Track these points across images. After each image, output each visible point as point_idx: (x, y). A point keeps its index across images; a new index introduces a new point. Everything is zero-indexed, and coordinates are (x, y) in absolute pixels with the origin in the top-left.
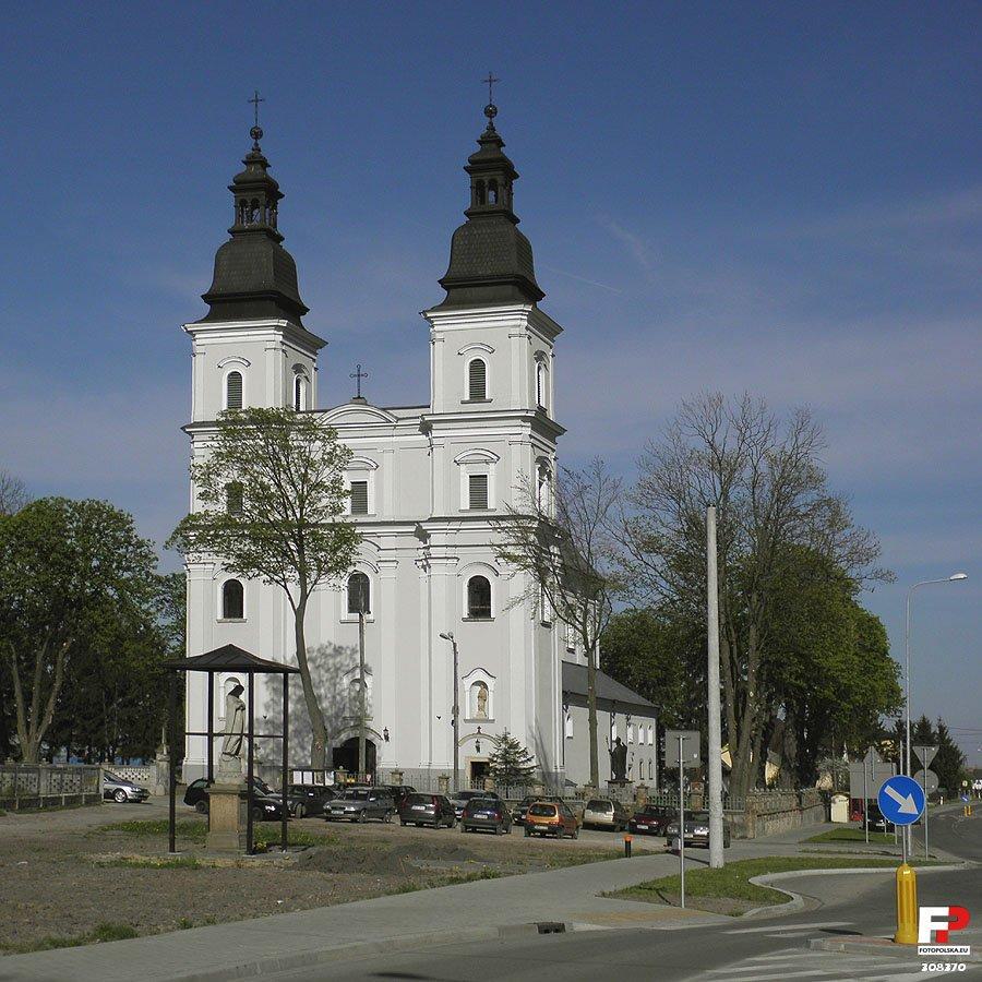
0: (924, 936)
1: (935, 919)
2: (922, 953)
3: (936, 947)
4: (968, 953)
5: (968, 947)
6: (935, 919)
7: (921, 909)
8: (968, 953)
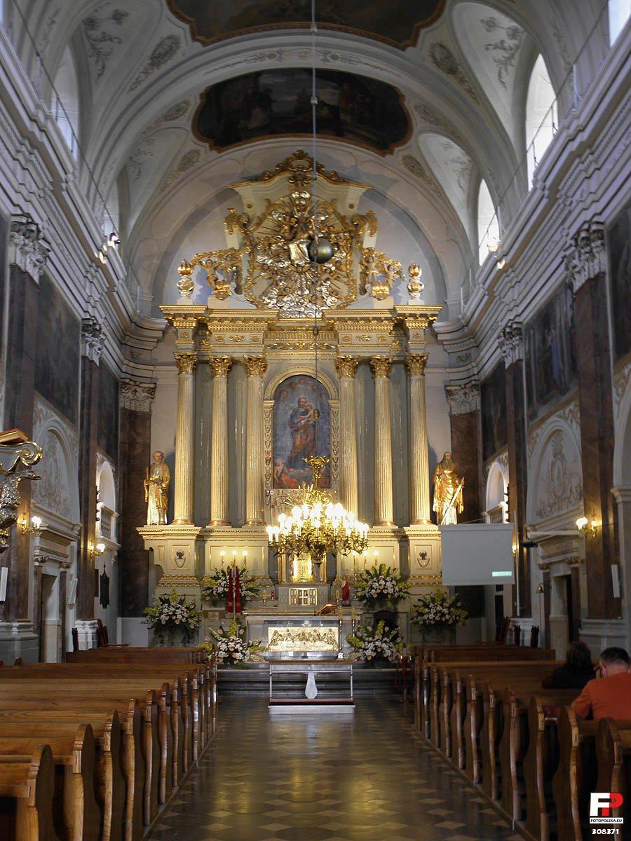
0: (594, 811)
1: (601, 800)
2: (592, 823)
3: (601, 819)
4: (622, 822)
5: (622, 819)
6: (601, 800)
7: (592, 794)
8: (622, 822)
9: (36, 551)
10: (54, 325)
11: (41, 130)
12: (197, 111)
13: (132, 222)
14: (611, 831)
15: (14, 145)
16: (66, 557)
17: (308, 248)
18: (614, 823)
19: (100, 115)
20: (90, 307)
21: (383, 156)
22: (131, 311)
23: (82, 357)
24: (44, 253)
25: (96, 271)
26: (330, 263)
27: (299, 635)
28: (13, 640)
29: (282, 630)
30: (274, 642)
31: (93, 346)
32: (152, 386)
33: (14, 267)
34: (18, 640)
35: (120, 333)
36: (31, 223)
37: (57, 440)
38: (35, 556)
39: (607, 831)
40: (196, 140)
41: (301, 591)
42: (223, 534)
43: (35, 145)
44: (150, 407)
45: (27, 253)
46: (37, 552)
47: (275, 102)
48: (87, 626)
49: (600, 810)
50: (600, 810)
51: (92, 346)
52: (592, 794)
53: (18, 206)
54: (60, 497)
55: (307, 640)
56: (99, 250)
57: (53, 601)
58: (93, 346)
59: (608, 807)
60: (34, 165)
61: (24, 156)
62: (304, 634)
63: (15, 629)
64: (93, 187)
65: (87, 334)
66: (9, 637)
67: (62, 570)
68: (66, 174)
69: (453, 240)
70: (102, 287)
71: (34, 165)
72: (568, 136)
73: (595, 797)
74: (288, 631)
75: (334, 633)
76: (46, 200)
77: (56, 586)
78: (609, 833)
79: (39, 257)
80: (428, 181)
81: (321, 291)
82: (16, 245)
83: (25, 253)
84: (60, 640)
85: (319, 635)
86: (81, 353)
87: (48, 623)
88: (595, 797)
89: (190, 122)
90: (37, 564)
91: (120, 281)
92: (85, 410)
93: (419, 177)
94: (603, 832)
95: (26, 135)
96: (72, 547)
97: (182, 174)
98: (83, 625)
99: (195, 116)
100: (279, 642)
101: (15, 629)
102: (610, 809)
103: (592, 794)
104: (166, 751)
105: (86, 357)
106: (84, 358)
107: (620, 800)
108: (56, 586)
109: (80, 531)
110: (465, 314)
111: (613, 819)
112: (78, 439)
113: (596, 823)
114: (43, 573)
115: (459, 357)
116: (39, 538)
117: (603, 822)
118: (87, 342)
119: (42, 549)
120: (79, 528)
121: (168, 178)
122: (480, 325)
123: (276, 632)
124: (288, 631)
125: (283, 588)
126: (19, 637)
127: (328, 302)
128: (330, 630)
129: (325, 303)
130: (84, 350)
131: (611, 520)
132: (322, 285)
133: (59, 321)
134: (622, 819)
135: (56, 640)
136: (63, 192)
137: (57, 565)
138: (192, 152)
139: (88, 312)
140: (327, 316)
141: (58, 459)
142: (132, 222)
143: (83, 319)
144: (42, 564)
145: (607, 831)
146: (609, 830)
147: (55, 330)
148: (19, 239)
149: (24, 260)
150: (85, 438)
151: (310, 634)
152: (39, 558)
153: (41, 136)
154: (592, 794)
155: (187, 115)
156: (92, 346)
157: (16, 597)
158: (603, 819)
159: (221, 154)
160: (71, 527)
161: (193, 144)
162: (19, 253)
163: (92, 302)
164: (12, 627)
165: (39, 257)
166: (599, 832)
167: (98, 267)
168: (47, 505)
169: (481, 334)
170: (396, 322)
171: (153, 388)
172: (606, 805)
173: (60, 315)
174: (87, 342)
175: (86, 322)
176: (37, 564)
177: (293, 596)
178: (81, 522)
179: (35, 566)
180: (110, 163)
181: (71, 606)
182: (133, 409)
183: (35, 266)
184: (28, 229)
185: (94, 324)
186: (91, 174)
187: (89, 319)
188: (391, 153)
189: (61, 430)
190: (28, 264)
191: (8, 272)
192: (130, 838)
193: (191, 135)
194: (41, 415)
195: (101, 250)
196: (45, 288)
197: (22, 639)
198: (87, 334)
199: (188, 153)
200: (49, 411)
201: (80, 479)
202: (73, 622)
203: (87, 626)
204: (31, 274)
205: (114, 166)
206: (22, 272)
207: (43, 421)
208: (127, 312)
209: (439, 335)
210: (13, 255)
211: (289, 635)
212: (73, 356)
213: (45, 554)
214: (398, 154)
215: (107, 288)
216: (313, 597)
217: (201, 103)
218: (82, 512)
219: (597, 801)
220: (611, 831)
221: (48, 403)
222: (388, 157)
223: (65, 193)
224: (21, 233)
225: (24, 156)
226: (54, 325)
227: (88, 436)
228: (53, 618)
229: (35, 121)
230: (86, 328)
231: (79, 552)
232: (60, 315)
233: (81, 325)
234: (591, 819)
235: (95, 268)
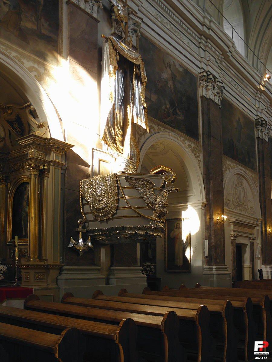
0: (256, 349)
1: (259, 345)
2: (255, 354)
3: (259, 352)
4: (268, 354)
5: (268, 352)
6: (259, 345)
7: (255, 342)
8: (268, 354)
9: (231, 232)
10: (235, 124)
11: (209, 29)
14: (264, 358)
15: (196, 40)
16: (253, 234)
18: (265, 354)
23: (257, 138)
24: (220, 88)
25: (261, 95)
28: (213, 274)
31: (263, 132)
33: (203, 97)
34: (215, 275)
36: (210, 75)
37: (243, 179)
38: (231, 234)
39: (262, 358)
43: (208, 37)
45: (209, 90)
46: (232, 232)
48: (268, 268)
49: (259, 349)
50: (259, 349)
51: (262, 132)
52: (255, 342)
53: (202, 68)
54: (248, 206)
56: (260, 84)
57: (247, 256)
58: (263, 132)
59: (262, 347)
60: (209, 48)
61: (203, 44)
63: (214, 269)
64: (256, 58)
65: (258, 126)
66: (211, 273)
67: (251, 241)
70: (266, 103)
71: (209, 48)
73: (256, 343)
76: (222, 64)
77: (248, 249)
78: (263, 358)
79: (218, 91)
82: (203, 87)
83: (208, 90)
84: (251, 275)
86: (256, 136)
87: (245, 267)
88: (256, 343)
90: (232, 238)
92: (261, 163)
94: (260, 358)
95: (201, 34)
96: (258, 230)
98: (265, 267)
101: (214, 269)
102: (263, 348)
103: (255, 342)
104: (226, 325)
106: (258, 138)
107: (267, 344)
108: (248, 249)
109: (262, 222)
111: (264, 352)
112: (257, 177)
113: (257, 354)
114: (236, 242)
116: (232, 226)
117: (260, 354)
118: (259, 130)
119: (234, 231)
120: (261, 221)
126: (216, 273)
130: (258, 134)
131: (264, 229)
134: (268, 352)
135: (249, 275)
136: (230, 58)
137: (248, 239)
139: (258, 116)
141: (245, 188)
143: (256, 120)
144: (235, 238)
145: (262, 358)
146: (263, 357)
148: (204, 83)
149: (208, 93)
150: (262, 176)
152: (233, 235)
153: (209, 32)
154: (255, 342)
157: (215, 254)
158: (260, 352)
160: (257, 220)
162: (204, 90)
163: (260, 110)
164: (213, 268)
165: (218, 91)
166: (258, 358)
167: (261, 93)
168: (238, 210)
172: (261, 347)
173: (239, 119)
174: (259, 130)
175: (257, 121)
176: (232, 238)
178: (262, 217)
179: (232, 239)
180: (264, 40)
181: (259, 258)
183: (266, 135)
184: (208, 78)
187: (259, 119)
189: (246, 175)
190: (212, 95)
191: (200, 100)
194: (230, 167)
195: (261, 84)
196: (227, 107)
197: (217, 274)
198: (258, 126)
200: (235, 165)
201: (260, 197)
202: (259, 265)
203: (268, 268)
204: (213, 99)
205: (267, 42)
206: (208, 99)
207: (231, 169)
210: (202, 91)
212: (251, 138)
213: (236, 233)
215: (270, 103)
219: (257, 345)
220: (264, 358)
221: (234, 161)
223: (231, 58)
224: (204, 80)
225: (203, 44)
226: (235, 124)
227: (263, 175)
228: (247, 264)
229: (204, 25)
230: (258, 123)
231: (262, 232)
232: (239, 119)
233: (255, 123)
234: (255, 352)
235: (260, 94)
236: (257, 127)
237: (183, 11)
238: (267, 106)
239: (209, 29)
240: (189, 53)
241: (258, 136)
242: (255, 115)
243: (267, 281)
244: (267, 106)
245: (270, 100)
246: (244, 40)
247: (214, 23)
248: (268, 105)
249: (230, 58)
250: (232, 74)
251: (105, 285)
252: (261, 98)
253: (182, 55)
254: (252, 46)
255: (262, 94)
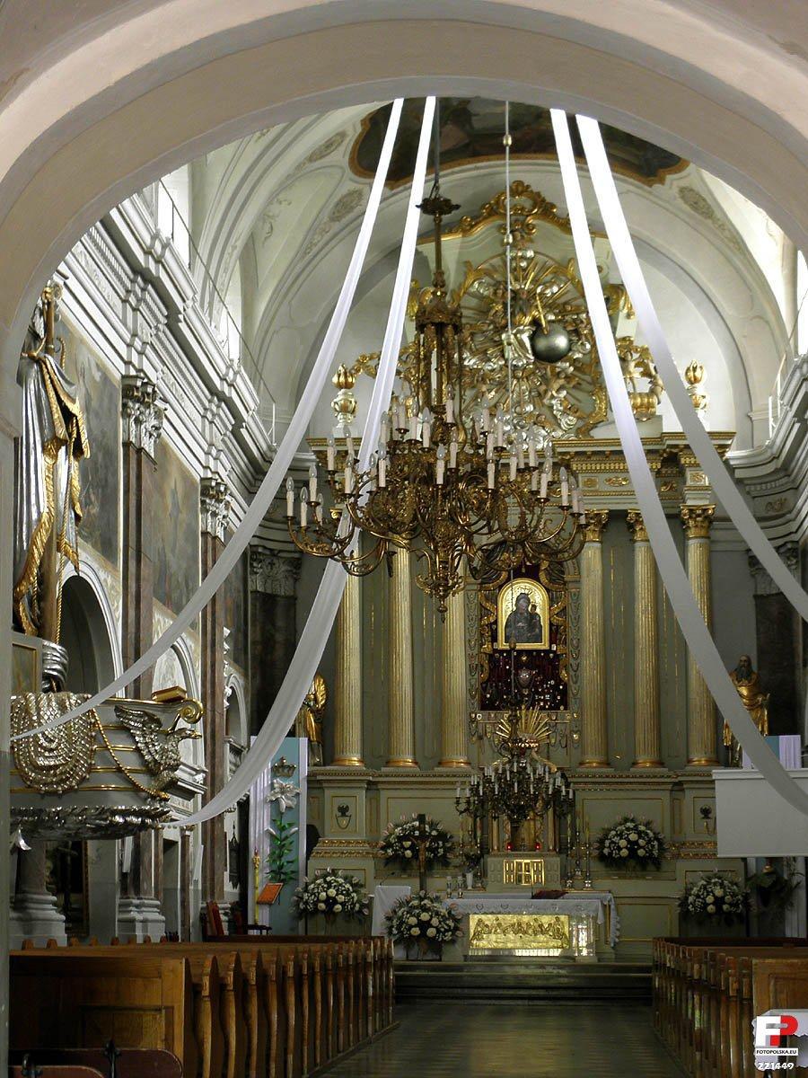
5: (797, 1049)
10: (169, 501)
12: (356, 142)
13: (261, 307)
17: (532, 338)
19: (218, 178)
20: (211, 459)
21: (651, 186)
22: (264, 447)
26: (566, 362)
27: (513, 925)
29: (489, 919)
30: (478, 935)
32: (297, 555)
35: (241, 468)
36: (147, 383)
40: (357, 178)
41: (521, 864)
42: (435, 779)
44: (294, 588)
47: (475, 115)
51: (138, 422)
55: (525, 933)
62: (520, 924)
64: (210, 284)
68: (184, 301)
69: (760, 317)
72: (772, 454)
74: (497, 919)
75: (562, 923)
80: (720, 226)
81: (551, 407)
85: (541, 926)
89: (347, 158)
91: (251, 412)
93: (706, 218)
95: (138, 270)
97: (336, 226)
99: (352, 152)
100: (485, 936)
105: (208, 533)
106: (205, 534)
110: (774, 442)
111: (785, 1049)
115: (770, 503)
118: (256, 573)
121: (314, 234)
122: (796, 459)
123: (480, 921)
124: (497, 919)
125: (493, 859)
127: (564, 426)
128: (558, 919)
129: (559, 425)
132: (553, 397)
133: (174, 492)
136: (180, 324)
138: (350, 194)
140: (559, 450)
142: (261, 307)
143: (202, 479)
147: (170, 507)
151: (528, 925)
153: (147, 261)
155: (342, 149)
156: (214, 515)
159: (394, 191)
161: (351, 183)
169: (799, 471)
170: (665, 455)
171: (298, 559)
174: (208, 511)
177: (510, 872)
178: (206, 766)
180: (232, 241)
182: (269, 591)
183: (151, 435)
185: (218, 484)
186: (207, 268)
188: (662, 181)
192: (291, 1075)
193: (348, 172)
199: (345, 196)
208: (258, 448)
209: (736, 471)
211: (499, 925)
214: (671, 184)
216: (537, 872)
217: (363, 129)
218: (208, 753)
222: (657, 186)
223: (182, 326)
236: (251, 565)
237: (123, 232)
238: (157, 328)
239: (158, 261)
240: (111, 324)
241: (204, 529)
242: (201, 464)
243: (246, 932)
244: (157, 328)
245: (234, 418)
246: (240, 331)
247: (242, 377)
248: (160, 326)
249: (180, 324)
250: (96, 244)
251: (23, 935)
252: (219, 415)
253: (176, 435)
254: (204, 249)
255: (223, 404)
